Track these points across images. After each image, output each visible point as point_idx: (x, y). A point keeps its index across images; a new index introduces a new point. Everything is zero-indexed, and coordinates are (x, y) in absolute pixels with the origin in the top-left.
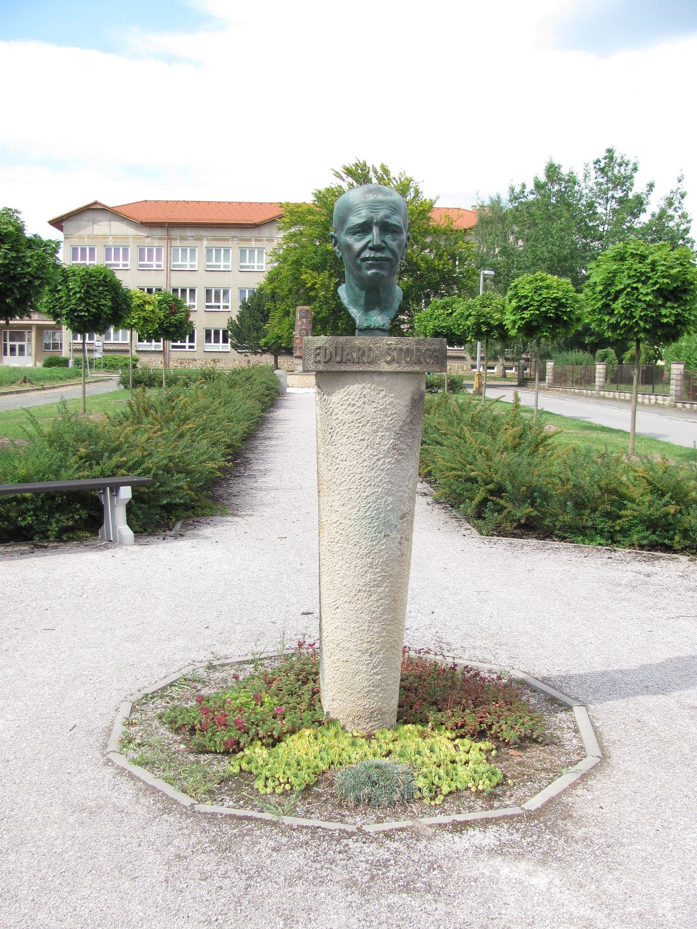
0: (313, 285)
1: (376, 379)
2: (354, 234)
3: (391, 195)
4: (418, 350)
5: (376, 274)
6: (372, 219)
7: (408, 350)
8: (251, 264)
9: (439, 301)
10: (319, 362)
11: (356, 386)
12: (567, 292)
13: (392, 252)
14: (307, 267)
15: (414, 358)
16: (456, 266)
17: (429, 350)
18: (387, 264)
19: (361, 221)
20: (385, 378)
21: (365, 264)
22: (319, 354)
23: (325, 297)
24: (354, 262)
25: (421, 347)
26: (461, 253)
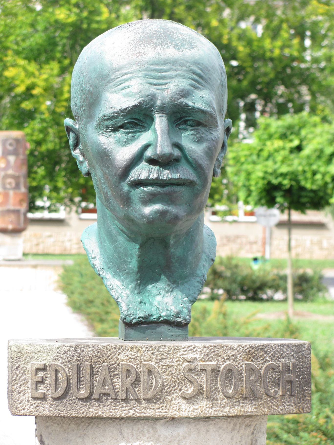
0: (30, 88)
2: (115, 130)
3: (192, 46)
4: (251, 370)
5: (162, 214)
6: (153, 98)
9: (276, 124)
10: (44, 398)
13: (197, 167)
14: (17, 53)
15: (244, 387)
16: (304, 49)
17: (273, 368)
18: (183, 191)
19: (131, 102)
20: (182, 430)
22: (42, 382)
23: (53, 113)
24: (116, 188)
25: (256, 364)
26: (315, 24)
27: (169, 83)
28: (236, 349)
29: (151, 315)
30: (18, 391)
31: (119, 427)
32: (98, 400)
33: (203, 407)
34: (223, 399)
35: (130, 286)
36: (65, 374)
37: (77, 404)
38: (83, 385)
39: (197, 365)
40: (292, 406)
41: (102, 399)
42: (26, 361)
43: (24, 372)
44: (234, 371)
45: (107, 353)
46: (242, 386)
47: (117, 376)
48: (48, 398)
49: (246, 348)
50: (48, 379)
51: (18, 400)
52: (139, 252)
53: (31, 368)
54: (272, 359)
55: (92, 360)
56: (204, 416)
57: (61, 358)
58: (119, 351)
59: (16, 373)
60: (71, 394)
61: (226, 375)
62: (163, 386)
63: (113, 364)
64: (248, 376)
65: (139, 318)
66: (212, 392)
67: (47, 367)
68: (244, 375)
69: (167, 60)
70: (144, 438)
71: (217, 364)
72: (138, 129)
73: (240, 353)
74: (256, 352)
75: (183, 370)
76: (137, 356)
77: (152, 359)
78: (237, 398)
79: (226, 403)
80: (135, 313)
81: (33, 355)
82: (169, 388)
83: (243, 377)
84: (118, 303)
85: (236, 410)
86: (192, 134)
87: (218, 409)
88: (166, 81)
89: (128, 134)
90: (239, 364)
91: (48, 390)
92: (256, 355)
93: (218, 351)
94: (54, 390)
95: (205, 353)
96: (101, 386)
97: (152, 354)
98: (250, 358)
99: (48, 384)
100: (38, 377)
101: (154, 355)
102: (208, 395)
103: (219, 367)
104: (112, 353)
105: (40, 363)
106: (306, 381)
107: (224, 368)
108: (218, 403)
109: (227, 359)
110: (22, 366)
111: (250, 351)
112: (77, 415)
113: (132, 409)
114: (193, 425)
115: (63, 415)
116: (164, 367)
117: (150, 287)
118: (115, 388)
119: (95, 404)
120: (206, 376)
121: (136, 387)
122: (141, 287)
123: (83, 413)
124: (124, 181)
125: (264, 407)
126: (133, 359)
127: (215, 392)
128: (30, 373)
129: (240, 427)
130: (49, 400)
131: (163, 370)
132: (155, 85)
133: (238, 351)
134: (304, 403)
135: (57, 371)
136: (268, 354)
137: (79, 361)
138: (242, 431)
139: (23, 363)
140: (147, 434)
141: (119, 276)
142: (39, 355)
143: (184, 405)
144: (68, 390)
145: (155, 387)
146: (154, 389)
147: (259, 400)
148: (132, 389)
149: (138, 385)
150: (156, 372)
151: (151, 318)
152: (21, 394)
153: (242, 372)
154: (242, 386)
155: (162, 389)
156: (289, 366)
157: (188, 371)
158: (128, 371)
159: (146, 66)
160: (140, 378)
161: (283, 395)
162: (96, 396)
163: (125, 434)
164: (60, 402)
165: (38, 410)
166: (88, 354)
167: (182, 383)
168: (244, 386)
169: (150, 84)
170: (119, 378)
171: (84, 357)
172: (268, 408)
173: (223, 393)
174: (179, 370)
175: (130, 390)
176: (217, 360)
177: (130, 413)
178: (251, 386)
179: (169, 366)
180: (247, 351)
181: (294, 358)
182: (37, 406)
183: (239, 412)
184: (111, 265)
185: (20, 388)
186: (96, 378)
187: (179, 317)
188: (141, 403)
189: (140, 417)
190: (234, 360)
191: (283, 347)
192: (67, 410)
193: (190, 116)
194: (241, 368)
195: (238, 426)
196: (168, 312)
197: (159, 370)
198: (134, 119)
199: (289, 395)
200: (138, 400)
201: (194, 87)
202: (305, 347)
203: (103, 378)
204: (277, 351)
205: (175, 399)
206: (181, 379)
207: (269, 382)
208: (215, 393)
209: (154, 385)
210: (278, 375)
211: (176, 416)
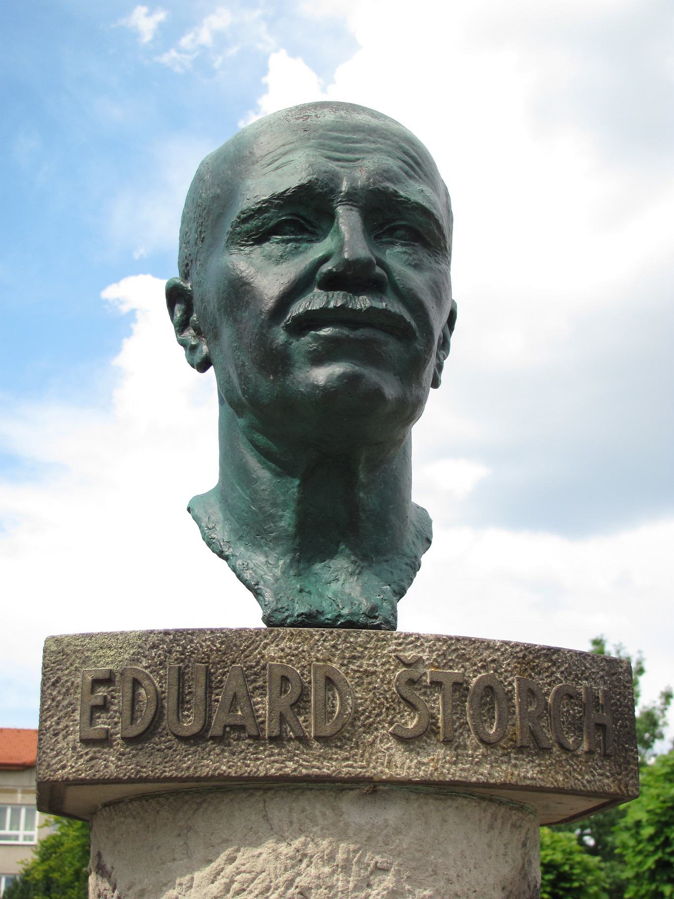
1: (356, 814)
2: (260, 238)
5: (350, 381)
7: (489, 690)
8: (14, 832)
10: (105, 741)
11: (266, 849)
12: (571, 853)
20: (392, 814)
21: (306, 342)
22: (104, 707)
27: (363, 158)
28: (498, 650)
29: (322, 613)
30: (54, 730)
31: (261, 805)
32: (219, 740)
33: (438, 760)
34: (476, 748)
35: (281, 562)
36: (151, 688)
37: (175, 751)
38: (188, 710)
39: (425, 674)
40: (608, 777)
41: (229, 737)
42: (73, 668)
43: (67, 690)
44: (498, 688)
45: (241, 645)
46: (514, 725)
47: (261, 691)
48: (115, 740)
49: (518, 649)
50: (116, 701)
51: (53, 750)
52: (299, 492)
53: (84, 678)
54: (565, 678)
55: (209, 658)
56: (441, 778)
57: (145, 657)
58: (266, 641)
59: (51, 694)
60: (163, 729)
61: (482, 698)
62: (357, 712)
63: (252, 667)
64: (523, 706)
65: (298, 616)
66: (456, 731)
67: (115, 676)
68: (516, 701)
69: (359, 126)
70: (314, 829)
71: (463, 674)
72: (305, 237)
73: (506, 659)
74: (537, 661)
75: (397, 680)
76: (303, 651)
77: (332, 658)
78: (504, 748)
79: (483, 755)
80: (291, 607)
81: (89, 654)
82: (369, 717)
83: (514, 706)
84: (259, 591)
85: (503, 771)
86: (405, 252)
87: (467, 766)
88: (357, 156)
89: (287, 243)
90: (505, 679)
91: (116, 723)
92: (537, 665)
93: (464, 649)
94: (128, 721)
95: (439, 650)
96: (227, 711)
97: (333, 646)
98: (526, 669)
99: (116, 711)
100: (96, 697)
101: (337, 649)
102: (449, 736)
103: (468, 683)
104: (251, 644)
105: (104, 667)
106: (629, 733)
107: (478, 682)
108: (468, 755)
109: (483, 667)
110: (65, 678)
111: (524, 657)
112: (175, 774)
113: (291, 759)
114: (416, 805)
115: (144, 775)
116: (358, 675)
117: (318, 567)
118: (256, 714)
119: (214, 749)
120: (443, 697)
121: (300, 714)
122: (301, 566)
123: (188, 768)
124: (278, 324)
125: (557, 773)
126: (293, 656)
127: (461, 731)
128: (79, 691)
129: (503, 824)
130: (118, 744)
131: (357, 680)
132: (338, 160)
133: (503, 654)
134: (627, 775)
135: (136, 683)
136: (558, 668)
137: (182, 661)
138: (506, 834)
139: (66, 672)
140: (321, 821)
141: (260, 546)
142: (101, 653)
143: (399, 755)
144: (157, 722)
145: (339, 713)
146: (337, 717)
147: (547, 757)
148: (292, 715)
149: (305, 709)
150: (342, 683)
151: (323, 618)
152: (60, 737)
153: (513, 695)
154: (514, 725)
155: (355, 719)
156: (598, 697)
157: (407, 683)
158: (285, 679)
159: (321, 131)
160: (308, 695)
161: (590, 752)
162: (216, 730)
163: (275, 822)
164: (139, 747)
165: (92, 766)
166: (202, 646)
167: (394, 709)
168: (518, 723)
169: (329, 158)
170: (265, 695)
171: (194, 653)
172: (564, 775)
173: (477, 733)
174: (389, 683)
175: (288, 718)
176: (463, 667)
177: (286, 767)
178: (530, 724)
179: (367, 673)
180: (521, 655)
181: (605, 683)
182: (92, 759)
183: (509, 777)
184: (244, 530)
185: (58, 724)
186: (217, 695)
187: (376, 617)
188: (311, 748)
189: (307, 775)
190: (495, 671)
191: (584, 658)
192: (153, 763)
193: (402, 220)
194: (510, 688)
195: (499, 821)
196: (355, 607)
197: (348, 679)
198: (299, 216)
199: (599, 754)
200: (303, 740)
201: (406, 173)
202: (622, 667)
203: (231, 693)
204: (575, 665)
205: (381, 742)
206: (393, 701)
207: (563, 722)
208: (461, 734)
209: (337, 709)
210: (579, 712)
211: (384, 777)
